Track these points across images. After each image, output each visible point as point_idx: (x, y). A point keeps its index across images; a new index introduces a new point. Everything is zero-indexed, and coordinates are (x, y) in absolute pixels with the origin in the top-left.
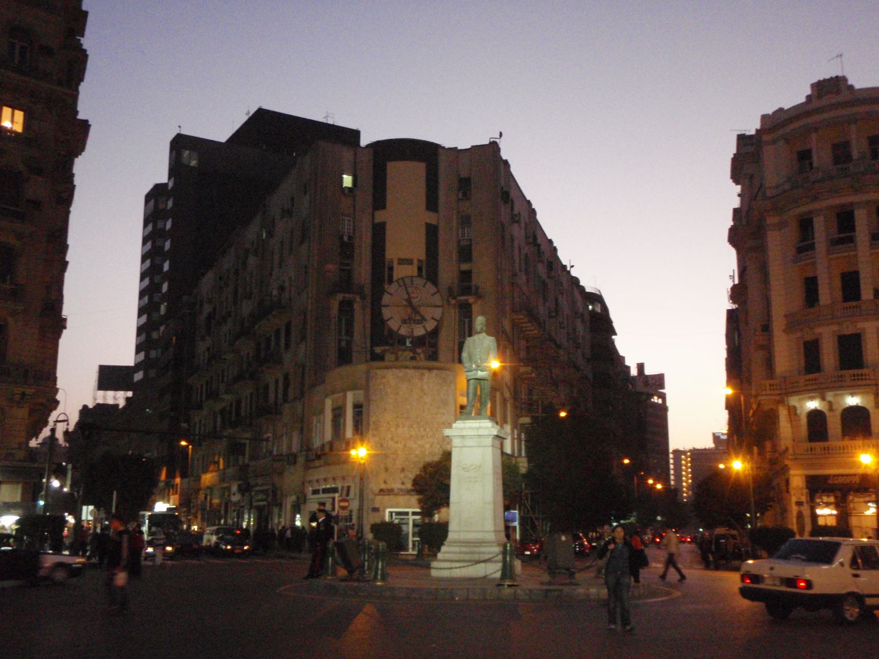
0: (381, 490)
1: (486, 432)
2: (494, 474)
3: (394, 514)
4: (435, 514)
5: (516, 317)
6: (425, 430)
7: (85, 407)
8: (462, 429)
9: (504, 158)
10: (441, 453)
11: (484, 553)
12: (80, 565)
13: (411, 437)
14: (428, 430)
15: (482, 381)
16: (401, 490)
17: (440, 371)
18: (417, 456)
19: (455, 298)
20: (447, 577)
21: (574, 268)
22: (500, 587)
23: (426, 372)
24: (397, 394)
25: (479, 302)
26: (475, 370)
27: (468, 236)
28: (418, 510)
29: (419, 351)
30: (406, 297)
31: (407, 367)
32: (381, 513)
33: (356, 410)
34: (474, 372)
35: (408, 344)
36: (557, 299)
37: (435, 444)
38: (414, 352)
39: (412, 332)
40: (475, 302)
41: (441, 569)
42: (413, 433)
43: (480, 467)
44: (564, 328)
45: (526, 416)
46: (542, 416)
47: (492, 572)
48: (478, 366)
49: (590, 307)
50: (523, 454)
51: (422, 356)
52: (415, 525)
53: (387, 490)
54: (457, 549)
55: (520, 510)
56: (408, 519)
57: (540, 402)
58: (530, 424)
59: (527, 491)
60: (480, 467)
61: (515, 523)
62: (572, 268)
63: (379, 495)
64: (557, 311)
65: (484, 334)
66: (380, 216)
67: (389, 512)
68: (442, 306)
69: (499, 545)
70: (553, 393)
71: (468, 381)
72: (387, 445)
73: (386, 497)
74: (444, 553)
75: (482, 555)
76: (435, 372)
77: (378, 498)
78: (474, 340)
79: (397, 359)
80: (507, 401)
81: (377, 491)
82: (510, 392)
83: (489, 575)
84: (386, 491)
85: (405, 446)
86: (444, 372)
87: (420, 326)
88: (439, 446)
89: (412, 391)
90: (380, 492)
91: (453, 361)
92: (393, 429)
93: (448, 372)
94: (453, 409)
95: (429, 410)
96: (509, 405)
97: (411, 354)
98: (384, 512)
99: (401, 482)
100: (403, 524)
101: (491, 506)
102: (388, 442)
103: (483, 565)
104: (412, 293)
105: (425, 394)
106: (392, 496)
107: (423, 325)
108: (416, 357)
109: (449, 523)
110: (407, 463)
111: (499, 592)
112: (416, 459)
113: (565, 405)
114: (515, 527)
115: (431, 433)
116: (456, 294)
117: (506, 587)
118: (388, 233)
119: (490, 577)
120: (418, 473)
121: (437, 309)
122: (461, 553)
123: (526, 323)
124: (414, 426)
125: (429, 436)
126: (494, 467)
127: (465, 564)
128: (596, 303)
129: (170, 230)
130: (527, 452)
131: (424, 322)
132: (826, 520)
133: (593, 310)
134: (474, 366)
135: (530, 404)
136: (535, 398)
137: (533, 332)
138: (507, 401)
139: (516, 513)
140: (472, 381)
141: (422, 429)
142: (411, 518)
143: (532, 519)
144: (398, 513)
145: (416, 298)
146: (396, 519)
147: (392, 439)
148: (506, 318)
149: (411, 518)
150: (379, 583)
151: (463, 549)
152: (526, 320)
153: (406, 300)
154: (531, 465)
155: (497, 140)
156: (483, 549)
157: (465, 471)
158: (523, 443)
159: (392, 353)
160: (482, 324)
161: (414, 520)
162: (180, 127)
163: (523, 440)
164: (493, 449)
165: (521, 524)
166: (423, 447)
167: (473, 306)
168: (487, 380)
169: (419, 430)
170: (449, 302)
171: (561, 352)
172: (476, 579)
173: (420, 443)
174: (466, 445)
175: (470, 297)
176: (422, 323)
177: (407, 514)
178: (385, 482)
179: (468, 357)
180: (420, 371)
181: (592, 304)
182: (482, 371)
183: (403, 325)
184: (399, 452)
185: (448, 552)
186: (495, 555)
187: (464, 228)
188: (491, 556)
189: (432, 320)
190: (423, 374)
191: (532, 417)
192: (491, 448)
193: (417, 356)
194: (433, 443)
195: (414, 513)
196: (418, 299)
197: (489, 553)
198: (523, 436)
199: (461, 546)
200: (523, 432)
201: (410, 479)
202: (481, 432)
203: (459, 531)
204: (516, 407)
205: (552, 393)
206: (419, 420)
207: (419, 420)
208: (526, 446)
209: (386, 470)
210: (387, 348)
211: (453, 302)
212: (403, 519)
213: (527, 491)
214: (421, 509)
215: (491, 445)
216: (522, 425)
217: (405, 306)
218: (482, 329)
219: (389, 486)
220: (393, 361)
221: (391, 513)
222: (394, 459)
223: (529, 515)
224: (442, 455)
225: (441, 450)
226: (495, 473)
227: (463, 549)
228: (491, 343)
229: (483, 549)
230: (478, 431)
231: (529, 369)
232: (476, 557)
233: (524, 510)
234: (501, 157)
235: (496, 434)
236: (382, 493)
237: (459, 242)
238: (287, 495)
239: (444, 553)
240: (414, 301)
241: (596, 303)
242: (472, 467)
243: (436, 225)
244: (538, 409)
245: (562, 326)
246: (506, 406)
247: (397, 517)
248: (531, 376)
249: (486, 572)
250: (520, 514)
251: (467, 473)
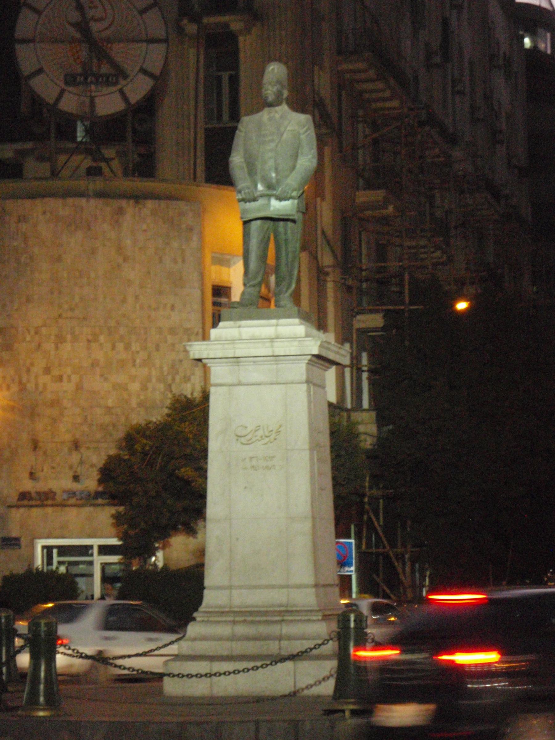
0: (24, 496)
1: (292, 348)
2: (311, 450)
3: (55, 551)
4: (157, 549)
5: (346, 66)
6: (127, 347)
8: (233, 341)
10: (168, 402)
11: (290, 638)
13: (95, 364)
14: (135, 347)
15: (281, 223)
16: (72, 494)
17: (163, 203)
18: (109, 410)
19: (196, 19)
20: (202, 698)
22: (332, 717)
23: (129, 207)
24: (59, 259)
25: (256, 30)
26: (262, 196)
28: (114, 541)
29: (109, 152)
30: (75, 16)
31: (81, 195)
32: (23, 551)
34: (261, 202)
35: (80, 135)
36: (445, 23)
37: (154, 380)
38: (97, 156)
39: (92, 105)
40: (248, 30)
41: (190, 676)
42: (100, 356)
43: (278, 432)
44: (461, 93)
45: (371, 311)
46: (410, 310)
47: (312, 682)
48: (270, 186)
49: (527, 41)
50: (366, 404)
51: (115, 164)
52: (105, 579)
53: (38, 493)
54: (225, 630)
55: (358, 538)
56: (91, 563)
57: (406, 276)
58: (383, 329)
59: (375, 492)
60: (278, 432)
61: (347, 569)
63: (18, 507)
64: (446, 57)
65: (285, 107)
67: (44, 547)
68: (166, 41)
69: (326, 618)
70: (438, 253)
71: (246, 223)
72: (37, 385)
73: (36, 512)
74: (194, 639)
75: (284, 643)
76: (150, 204)
77: (17, 515)
78: (260, 125)
79: (54, 174)
80: (327, 274)
81: (13, 498)
82: (333, 252)
83: (303, 690)
84: (34, 495)
85: (79, 387)
86: (174, 202)
87: (112, 89)
88: (162, 386)
89: (94, 252)
90: (19, 500)
91: (195, 179)
92: (49, 346)
93: (181, 204)
94: (197, 293)
95: (137, 298)
96: (330, 286)
97: (88, 163)
98: (32, 547)
99: (71, 474)
100: (77, 575)
101: (307, 526)
102: (36, 377)
103: (289, 665)
104: (90, 8)
105: (125, 260)
106: (49, 510)
107: (119, 87)
108: (100, 169)
109: (206, 566)
110: (85, 428)
111: (332, 727)
112: (107, 419)
113: (463, 284)
114: (350, 577)
115: (143, 355)
116: (197, 8)
117: (347, 714)
119: (306, 692)
120: (113, 452)
121: (152, 46)
122: (233, 638)
123: (371, 80)
124: (102, 338)
125: (138, 361)
126: (313, 429)
127: (251, 665)
128: (540, 31)
130: (373, 398)
131: (123, 82)
132: (231, 596)
133: (535, 49)
134: (260, 187)
135: (381, 283)
136: (393, 265)
137: (388, 104)
138: (327, 274)
139: (351, 543)
140: (255, 225)
141: (120, 346)
142: (98, 560)
143: (386, 557)
144: (63, 550)
145: (101, 19)
146: (60, 563)
147: (47, 370)
148: (321, 68)
149: (98, 560)
150: (41, 714)
151: (241, 630)
152: (371, 74)
153: (76, 25)
154: (385, 429)
156: (286, 629)
157: (242, 443)
158: (365, 375)
159: (41, 159)
160: (279, 82)
161: (104, 566)
163: (365, 368)
164: (309, 390)
165: (358, 570)
166: (126, 389)
167: (241, 39)
168: (294, 221)
169: (114, 348)
170: (180, 30)
171: (457, 153)
172: (273, 699)
173: (121, 378)
174: (244, 380)
175: (233, 17)
176: (117, 83)
177: (85, 550)
178: (32, 475)
179: (244, 165)
180: (115, 203)
181: (534, 36)
182: (280, 199)
183: (70, 89)
184: (66, 403)
185: (204, 638)
186: (320, 642)
188: (311, 644)
189: (141, 76)
190: (121, 211)
191: (387, 314)
192: (304, 387)
193: (103, 165)
194: (149, 380)
195: (104, 550)
196: (106, 24)
197: (303, 638)
198: (365, 360)
199: (234, 622)
200: (364, 350)
201: (93, 466)
202: (280, 349)
203: (230, 587)
204: (349, 289)
205: (435, 255)
206: (112, 323)
207: (112, 323)
208: (372, 383)
209: (35, 445)
210: (29, 145)
211: (191, 28)
212: (77, 563)
213: (375, 492)
214: (120, 539)
215: (304, 378)
216: (362, 332)
217: (73, 41)
218: (279, 94)
219: (42, 486)
220: (46, 179)
221: (48, 549)
222: (54, 420)
223: (381, 550)
224: (173, 407)
225: (170, 396)
226: (314, 446)
227: (241, 630)
228: (302, 131)
229: (286, 629)
230: (272, 346)
231: (379, 195)
232: (273, 647)
233: (369, 540)
235: (316, 352)
236: (25, 502)
239: (194, 639)
240: (95, 27)
241: (540, 31)
242: (260, 433)
244: (401, 293)
245: (458, 88)
246: (325, 289)
247: (62, 559)
248: (384, 212)
249: (295, 686)
250: (358, 546)
251: (247, 448)
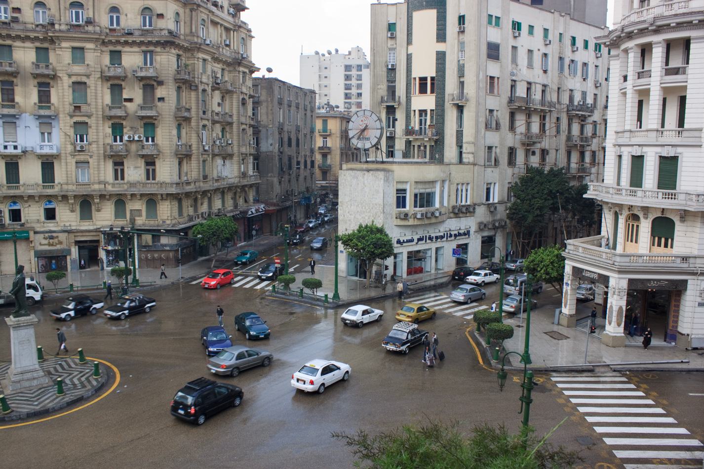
24: (351, 186)
85: (355, 217)
92: (349, 207)
180: (363, 172)
190: (364, 174)
237: (459, 61)
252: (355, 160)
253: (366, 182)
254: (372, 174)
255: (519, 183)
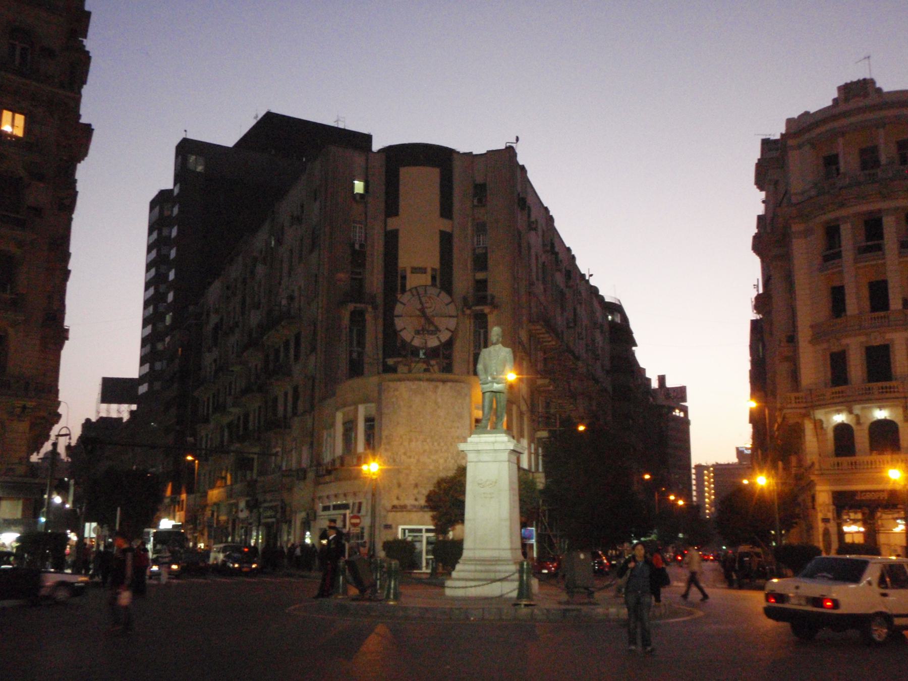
0: (394, 507)
1: (502, 447)
2: (510, 490)
3: (407, 531)
4: (449, 531)
5: (533, 327)
6: (439, 444)
7: (88, 421)
8: (477, 443)
9: (521, 163)
10: (456, 468)
11: (499, 571)
12: (82, 584)
13: (425, 451)
14: (442, 444)
15: (498, 394)
16: (414, 506)
17: (455, 383)
18: (431, 471)
19: (470, 308)
20: (462, 597)
21: (593, 277)
22: (516, 607)
23: (440, 385)
24: (410, 407)
25: (495, 313)
26: (490, 382)
27: (483, 244)
28: (432, 527)
29: (433, 362)
30: (420, 307)
31: (420, 380)
32: (394, 530)
33: (367, 423)
34: (489, 385)
35: (422, 355)
36: (575, 309)
37: (450, 459)
38: (428, 364)
39: (426, 343)
40: (491, 312)
41: (455, 588)
42: (427, 447)
43: (496, 482)
44: (582, 339)
45: (543, 430)
46: (560, 430)
47: (509, 591)
48: (494, 378)
49: (610, 317)
50: (541, 469)
51: (436, 368)
52: (428, 543)
53: (400, 506)
54: (472, 568)
55: (537, 527)
56: (422, 536)
57: (558, 416)
58: (547, 438)
59: (545, 508)
60: (496, 482)
61: (532, 541)
62: (591, 277)
63: (391, 511)
64: (575, 321)
65: (500, 345)
66: (392, 223)
67: (402, 529)
68: (457, 317)
69: (515, 563)
70: (572, 406)
71: (484, 393)
72: (400, 460)
73: (399, 514)
74: (459, 571)
75: (497, 574)
76: (449, 384)
77: (391, 515)
78: (490, 352)
79: (410, 371)
80: (524, 414)
81: (389, 508)
82: (527, 405)
83: (505, 594)
84: (398, 507)
85: (418, 461)
86: (458, 384)
87: (433, 337)
88: (453, 461)
89: (425, 404)
90: (392, 508)
91: (468, 373)
92: (406, 444)
93: (462, 384)
94: (468, 422)
95: (443, 423)
96: (525, 419)
97: (425, 366)
98: (397, 529)
99: (414, 498)
100: (416, 541)
101: (508, 523)
102: (401, 456)
103: (499, 584)
104: (426, 303)
105: (439, 407)
106: (405, 513)
107: (437, 335)
108: (429, 369)
109: (464, 540)
110: (420, 478)
111: (516, 611)
112: (430, 475)
113: (583, 419)
114: (532, 544)
115: (445, 448)
116: (471, 304)
117: (523, 606)
118: (401, 240)
119: (506, 596)
120: (432, 489)
121: (451, 319)
122: (476, 571)
123: (543, 333)
124: (428, 440)
125: (443, 450)
126: (511, 482)
127: (481, 583)
128: (615, 313)
129: (176, 237)
130: (545, 467)
131: (438, 333)
133: (613, 320)
134: (489, 378)
135: (548, 418)
136: (552, 411)
137: (550, 343)
138: (524, 414)
139: (533, 530)
140: (487, 394)
141: (436, 444)
142: (425, 535)
143: (549, 536)
144: (411, 531)
145: (430, 308)
146: (409, 536)
147: (405, 454)
148: (523, 328)
149: (425, 535)
150: (391, 603)
151: (479, 568)
152: (543, 330)
153: (420, 310)
154: (548, 480)
155: (514, 145)
156: (499, 568)
157: (480, 487)
158: (540, 457)
159: (405, 365)
160: (498, 335)
161: (428, 538)
162: (185, 131)
163: (540, 454)
164: (509, 464)
165: (538, 542)
166: (437, 462)
167: (489, 316)
168: (503, 393)
169: (433, 445)
170: (463, 312)
171: (580, 364)
172: (492, 598)
173: (434, 457)
174: (482, 460)
175: (486, 307)
176: (436, 334)
177: (420, 531)
178: (398, 498)
179: (483, 369)
180: (434, 383)
181: (612, 314)
182: (498, 383)
183: (416, 336)
184: (412, 467)
185: (463, 571)
186: (511, 574)
187: (480, 236)
188: (507, 575)
189: (446, 331)
190: (437, 387)
191: (550, 431)
192: (507, 463)
193: (431, 368)
194: (448, 458)
195: (428, 531)
196: (432, 309)
197: (506, 572)
198: (540, 450)
199: (476, 564)
200: (540, 446)
201: (423, 495)
202: (497, 447)
203: (474, 549)
204: (533, 421)
205: (570, 406)
206: (433, 434)
207: (433, 434)
208: (543, 461)
209: (399, 485)
210: (400, 359)
211: (468, 312)
212: (417, 536)
213: (545, 508)
214: (434, 526)
215: (507, 459)
216: (540, 439)
217: (418, 316)
218: (498, 340)
219: (402, 503)
220: (406, 373)
221: (404, 530)
222: (407, 475)
223: (546, 533)
224: (457, 470)
225: (456, 465)
226: (511, 489)
227: (479, 568)
228: (507, 355)
229: (499, 568)
230: (494, 446)
231: (547, 381)
232: (492, 576)
233: (541, 527)
234: (517, 163)
235: (512, 448)
236: (394, 509)
237: (474, 250)
238: (296, 512)
239: (459, 571)
240: (428, 311)
241: (615, 313)
242: (488, 483)
243: (451, 232)
244: (556, 422)
245: (581, 337)
246: (523, 420)
247: (410, 534)
248: (549, 388)
249: (502, 591)
250: (537, 531)
251: (482, 489)
252: (180, 509)
253: (439, 400)
254: (451, 387)
255: (776, 503)
